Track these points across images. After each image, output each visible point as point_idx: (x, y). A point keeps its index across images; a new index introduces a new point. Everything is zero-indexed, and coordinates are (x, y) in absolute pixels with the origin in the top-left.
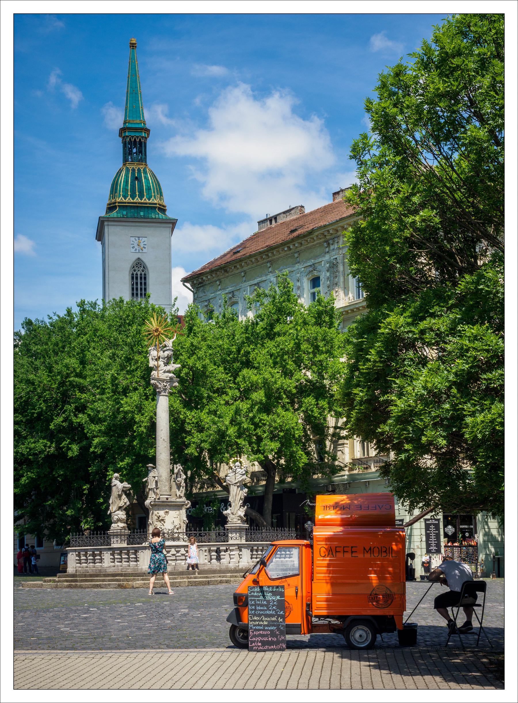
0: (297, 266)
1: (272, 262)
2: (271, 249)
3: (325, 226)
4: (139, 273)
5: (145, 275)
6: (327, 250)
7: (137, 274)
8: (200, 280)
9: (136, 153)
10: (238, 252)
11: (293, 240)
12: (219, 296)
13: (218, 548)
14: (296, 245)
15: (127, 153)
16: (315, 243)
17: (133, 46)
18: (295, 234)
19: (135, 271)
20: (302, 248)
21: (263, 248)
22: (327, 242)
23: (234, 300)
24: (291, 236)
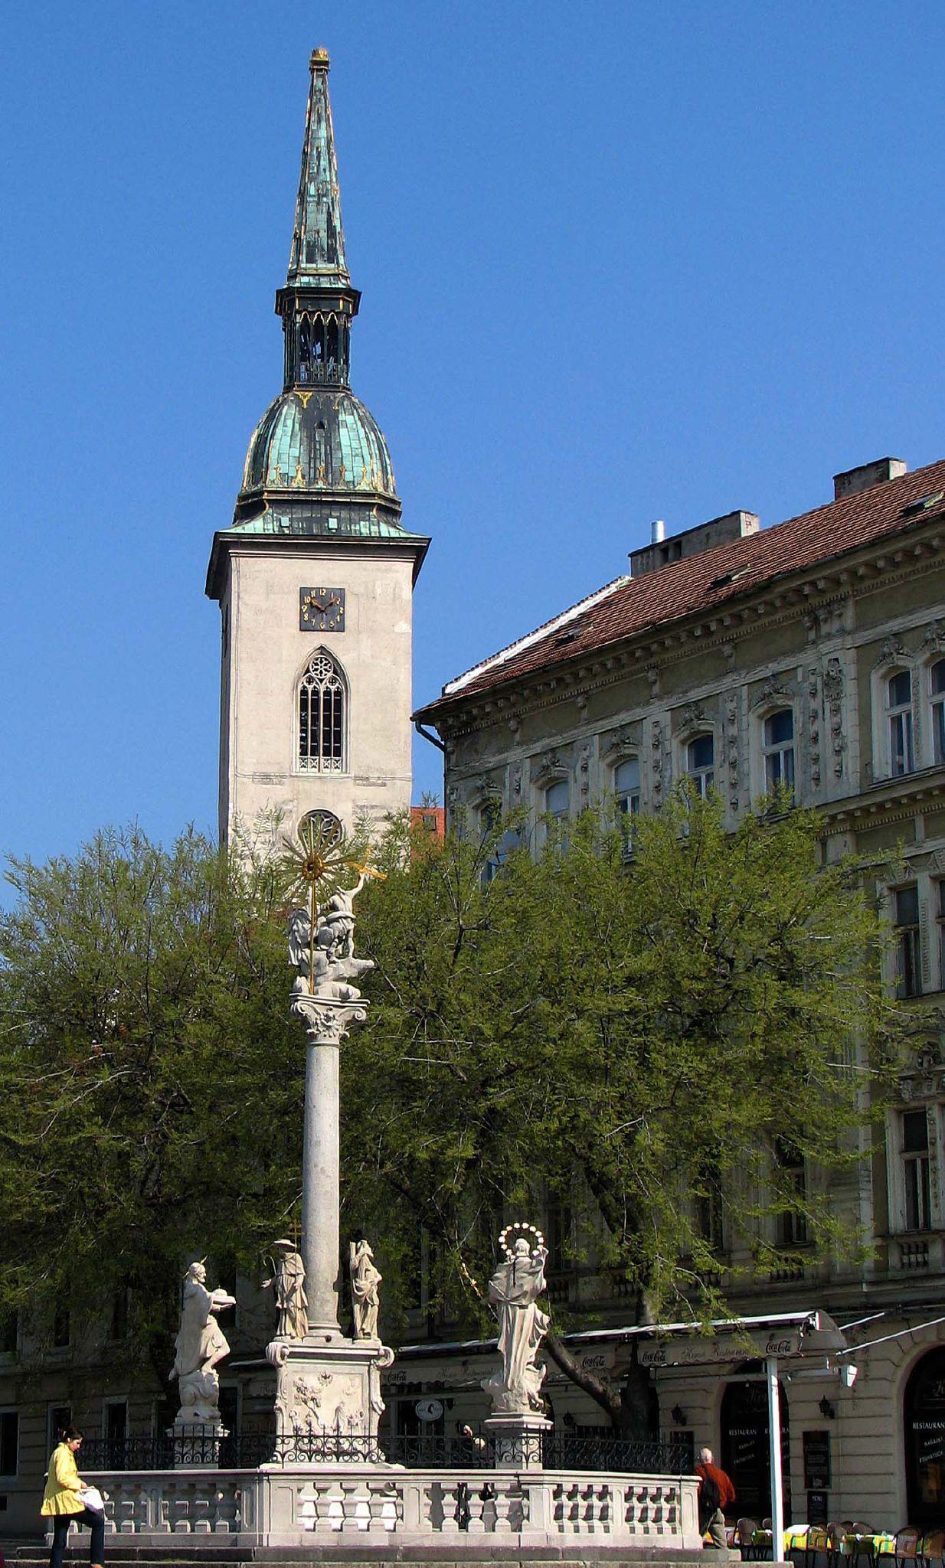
0: (728, 682)
1: (660, 669)
2: (657, 630)
3: (804, 571)
4: (322, 688)
5: (338, 693)
6: (812, 635)
7: (315, 692)
8: (464, 717)
9: (321, 356)
10: (571, 639)
11: (717, 607)
12: (516, 761)
13: (461, 1486)
14: (638, 654)
15: (297, 355)
16: (779, 616)
17: (319, 67)
18: (723, 592)
19: (310, 681)
20: (743, 629)
21: (635, 629)
22: (812, 613)
23: (555, 772)
24: (713, 598)
